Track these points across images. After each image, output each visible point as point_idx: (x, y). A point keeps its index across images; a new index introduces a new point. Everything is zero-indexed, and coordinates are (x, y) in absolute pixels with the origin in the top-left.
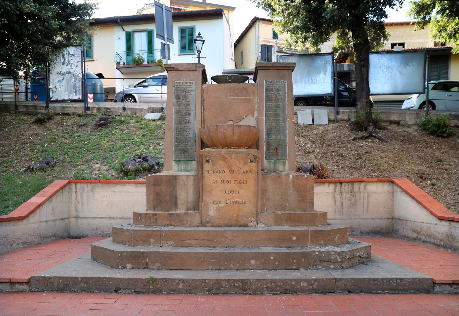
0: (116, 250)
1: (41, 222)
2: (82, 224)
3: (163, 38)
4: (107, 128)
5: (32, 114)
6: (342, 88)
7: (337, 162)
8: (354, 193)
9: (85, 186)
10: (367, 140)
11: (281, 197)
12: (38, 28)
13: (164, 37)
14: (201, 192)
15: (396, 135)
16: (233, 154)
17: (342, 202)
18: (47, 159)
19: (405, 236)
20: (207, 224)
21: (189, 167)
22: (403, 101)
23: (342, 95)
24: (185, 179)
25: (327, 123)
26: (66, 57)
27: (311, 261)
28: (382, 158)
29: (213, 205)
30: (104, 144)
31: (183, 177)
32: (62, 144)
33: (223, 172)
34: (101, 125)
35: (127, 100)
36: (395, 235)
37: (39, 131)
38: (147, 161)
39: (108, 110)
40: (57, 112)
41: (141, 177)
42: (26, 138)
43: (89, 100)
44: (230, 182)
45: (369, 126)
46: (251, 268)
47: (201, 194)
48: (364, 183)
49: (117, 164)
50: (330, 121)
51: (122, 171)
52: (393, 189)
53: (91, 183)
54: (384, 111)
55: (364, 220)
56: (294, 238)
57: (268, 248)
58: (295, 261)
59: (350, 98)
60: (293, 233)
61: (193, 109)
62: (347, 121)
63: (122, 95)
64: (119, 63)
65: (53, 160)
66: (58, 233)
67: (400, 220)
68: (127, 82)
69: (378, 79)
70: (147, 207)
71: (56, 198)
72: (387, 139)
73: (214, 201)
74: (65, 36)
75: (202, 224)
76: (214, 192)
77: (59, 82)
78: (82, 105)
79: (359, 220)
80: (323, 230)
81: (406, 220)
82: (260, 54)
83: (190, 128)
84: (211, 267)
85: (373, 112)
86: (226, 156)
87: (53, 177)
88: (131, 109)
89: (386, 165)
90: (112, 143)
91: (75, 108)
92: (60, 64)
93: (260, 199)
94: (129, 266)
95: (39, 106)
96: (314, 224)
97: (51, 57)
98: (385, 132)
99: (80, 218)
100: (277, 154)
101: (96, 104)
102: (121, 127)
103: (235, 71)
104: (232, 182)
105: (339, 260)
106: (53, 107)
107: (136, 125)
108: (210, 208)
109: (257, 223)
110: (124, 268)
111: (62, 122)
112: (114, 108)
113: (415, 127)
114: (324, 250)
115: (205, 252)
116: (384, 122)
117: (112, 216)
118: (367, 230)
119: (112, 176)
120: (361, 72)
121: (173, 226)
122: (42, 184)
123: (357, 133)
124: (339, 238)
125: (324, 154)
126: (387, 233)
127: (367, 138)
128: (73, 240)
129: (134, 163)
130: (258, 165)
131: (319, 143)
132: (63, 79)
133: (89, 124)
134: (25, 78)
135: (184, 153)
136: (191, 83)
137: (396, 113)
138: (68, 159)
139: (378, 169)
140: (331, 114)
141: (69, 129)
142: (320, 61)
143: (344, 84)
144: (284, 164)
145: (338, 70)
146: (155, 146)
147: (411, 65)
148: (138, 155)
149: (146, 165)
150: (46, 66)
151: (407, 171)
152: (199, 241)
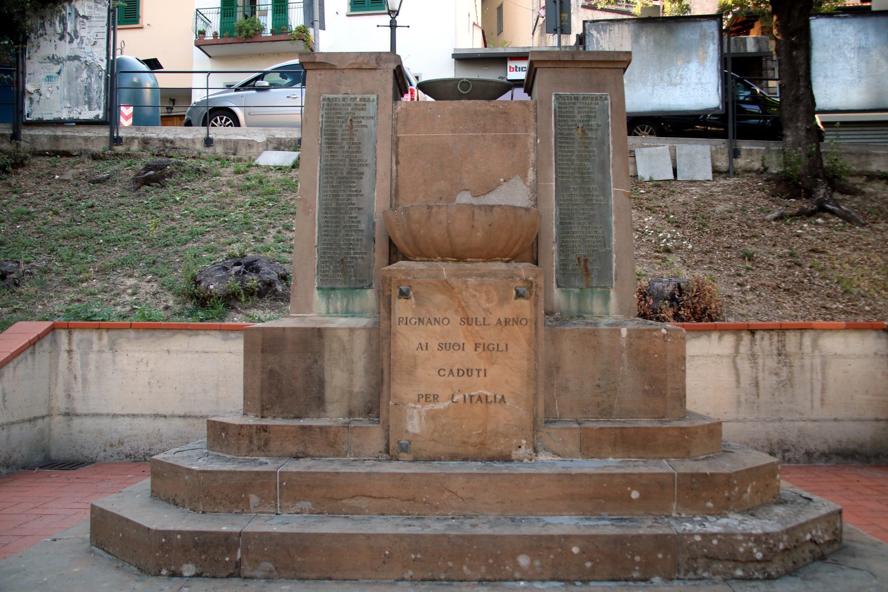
2: (81, 432)
4: (163, 186)
6: (744, 94)
7: (739, 275)
8: (786, 355)
9: (94, 335)
10: (812, 219)
11: (598, 382)
16: (470, 275)
17: (756, 378)
24: (344, 336)
25: (710, 177)
27: (682, 558)
28: (852, 264)
29: (419, 406)
30: (152, 227)
31: (340, 333)
32: (46, 227)
33: (446, 322)
34: (147, 181)
35: (216, 121)
38: (257, 270)
39: (169, 145)
40: (39, 148)
41: (239, 312)
43: (122, 120)
45: (816, 185)
46: (517, 575)
47: (386, 377)
48: (812, 332)
50: (716, 172)
51: (192, 296)
53: (108, 329)
56: (635, 495)
58: (637, 558)
59: (765, 119)
60: (631, 480)
61: (369, 161)
62: (759, 172)
64: (202, 33)
65: (19, 267)
66: (15, 456)
68: (218, 81)
69: (833, 76)
70: (245, 404)
71: (15, 368)
72: (865, 218)
73: (420, 396)
75: (389, 454)
76: (420, 372)
77: (49, 78)
78: (104, 132)
79: (802, 424)
80: (712, 474)
82: (543, 13)
83: (359, 209)
84: (411, 573)
85: (826, 153)
86: (453, 281)
87: (14, 311)
88: (225, 142)
89: (865, 284)
90: (173, 224)
91: (86, 139)
92: (53, 38)
93: (541, 389)
94: (189, 569)
96: (687, 455)
97: (29, 23)
98: (858, 199)
99: (77, 415)
100: (587, 273)
101: (138, 130)
102: (197, 185)
104: (470, 347)
105: (759, 556)
106: (31, 136)
107: (236, 180)
108: (409, 412)
109: (536, 451)
110: (174, 574)
111: (49, 174)
112: (182, 140)
114: (716, 529)
115: (395, 535)
116: (853, 175)
117: (162, 411)
118: (823, 448)
119: (167, 308)
120: (791, 60)
121: (312, 457)
123: (787, 202)
124: (756, 491)
125: (706, 252)
126: (877, 456)
127: (811, 214)
128: (55, 474)
129: (223, 277)
130: (536, 305)
131: (693, 227)
132: (59, 73)
135: (343, 270)
136: (364, 100)
137: (884, 155)
138: (57, 266)
139: (846, 292)
140: (719, 156)
141: (66, 190)
142: (688, 33)
143: (748, 87)
144: (606, 298)
145: (733, 50)
146: (279, 232)
148: (234, 257)
149: (253, 280)
150: (17, 43)
152: (381, 502)
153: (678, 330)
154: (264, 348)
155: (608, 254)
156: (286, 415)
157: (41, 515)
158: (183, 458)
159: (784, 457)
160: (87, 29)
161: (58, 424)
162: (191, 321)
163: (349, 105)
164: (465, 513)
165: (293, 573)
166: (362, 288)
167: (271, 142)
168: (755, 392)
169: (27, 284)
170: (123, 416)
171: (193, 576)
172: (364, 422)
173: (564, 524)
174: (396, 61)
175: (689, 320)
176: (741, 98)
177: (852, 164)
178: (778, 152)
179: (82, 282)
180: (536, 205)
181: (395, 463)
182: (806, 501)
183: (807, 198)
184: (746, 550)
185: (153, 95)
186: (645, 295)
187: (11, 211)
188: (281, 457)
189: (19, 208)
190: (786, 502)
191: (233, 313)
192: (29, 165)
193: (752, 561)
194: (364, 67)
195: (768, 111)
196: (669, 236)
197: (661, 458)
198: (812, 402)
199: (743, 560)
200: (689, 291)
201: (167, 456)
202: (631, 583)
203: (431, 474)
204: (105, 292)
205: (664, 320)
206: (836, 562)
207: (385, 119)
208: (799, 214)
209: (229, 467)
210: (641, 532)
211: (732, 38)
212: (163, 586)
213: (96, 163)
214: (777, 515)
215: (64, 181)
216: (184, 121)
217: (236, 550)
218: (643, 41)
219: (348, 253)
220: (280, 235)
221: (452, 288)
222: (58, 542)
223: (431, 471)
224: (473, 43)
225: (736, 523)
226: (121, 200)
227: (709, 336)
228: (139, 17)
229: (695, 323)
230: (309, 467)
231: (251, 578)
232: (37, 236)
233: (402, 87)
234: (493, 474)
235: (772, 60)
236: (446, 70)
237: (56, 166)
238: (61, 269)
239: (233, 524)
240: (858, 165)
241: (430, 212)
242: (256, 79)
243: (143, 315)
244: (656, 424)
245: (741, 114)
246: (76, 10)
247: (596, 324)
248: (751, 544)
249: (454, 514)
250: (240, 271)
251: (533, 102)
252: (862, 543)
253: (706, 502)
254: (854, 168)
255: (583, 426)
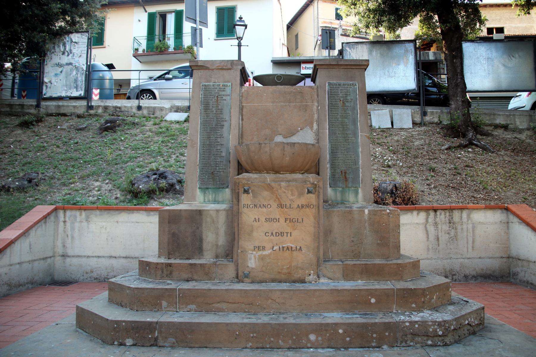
0: (110, 318)
1: (11, 265)
2: (70, 265)
3: (195, 21)
4: (115, 132)
5: (17, 115)
6: (428, 82)
7: (428, 180)
8: (453, 223)
9: (78, 213)
10: (466, 149)
11: (352, 239)
12: (33, 12)
13: (196, 21)
14: (236, 234)
15: (504, 142)
16: (282, 181)
17: (438, 236)
18: (30, 175)
19: (528, 282)
20: (245, 279)
21: (220, 197)
22: (510, 98)
23: (428, 91)
24: (213, 214)
26: (67, 46)
27: (399, 335)
28: (487, 173)
29: (254, 253)
31: (211, 213)
32: (52, 154)
33: (269, 206)
34: (106, 129)
35: (144, 97)
36: (512, 280)
37: (24, 137)
38: (166, 178)
39: (118, 110)
40: (50, 112)
41: (156, 201)
42: (5, 147)
43: (94, 96)
44: (278, 220)
45: (468, 131)
46: (309, 345)
48: (467, 210)
49: (124, 182)
50: (414, 123)
51: (130, 192)
52: (508, 217)
53: (85, 209)
54: (487, 111)
55: (469, 260)
56: (373, 301)
57: (335, 314)
58: (375, 335)
59: (440, 95)
60: (371, 293)
62: (437, 124)
63: (138, 91)
64: (137, 50)
65: (38, 176)
66: (36, 278)
67: (519, 260)
68: (145, 75)
69: (475, 73)
70: (159, 251)
71: (36, 231)
72: (494, 148)
74: (69, 21)
75: (238, 279)
76: (255, 234)
78: (84, 103)
79: (462, 260)
80: (415, 289)
81: (529, 261)
82: (320, 38)
83: (222, 145)
84: (250, 344)
85: (473, 114)
86: (273, 184)
87: (36, 200)
88: (148, 108)
89: (494, 184)
90: (120, 152)
91: (75, 107)
92: (59, 54)
93: (321, 243)
94: (129, 342)
95: (27, 105)
96: (401, 279)
97: (47, 46)
98: (490, 138)
99: (68, 256)
100: (346, 179)
101: (102, 102)
102: (134, 131)
103: (288, 59)
104: (282, 220)
105: (440, 333)
106: (46, 105)
107: (154, 128)
108: (249, 256)
109: (318, 277)
110: (121, 344)
111: (55, 125)
112: (125, 107)
113: (529, 133)
114: (417, 319)
115: (241, 324)
117: (114, 255)
118: (474, 273)
119: (116, 198)
121: (196, 280)
122: (20, 209)
123: (452, 140)
125: (410, 167)
126: (502, 277)
127: (466, 146)
128: (57, 288)
129: (147, 181)
130: (318, 197)
132: (61, 72)
133: (91, 128)
134: (13, 71)
135: (212, 178)
136: (224, 86)
137: (503, 115)
141: (64, 134)
142: (398, 50)
143: (430, 78)
144: (357, 193)
145: (422, 59)
147: (517, 56)
148: (153, 170)
149: (163, 183)
150: (41, 57)
151: (523, 192)
152: (234, 305)
153: (396, 211)
154: (169, 220)
155: (357, 169)
156: (181, 257)
157: (50, 311)
158: (126, 280)
159: (452, 279)
160: (77, 49)
161: (58, 260)
162: (129, 206)
163: (216, 88)
164: (280, 311)
165: (186, 344)
166: (223, 188)
167: (173, 108)
168: (437, 243)
169: (43, 185)
170: (93, 257)
171: (132, 345)
172: (224, 262)
173: (334, 317)
174: (241, 65)
175: (401, 204)
176: (427, 84)
177: (486, 120)
178: (447, 113)
179: (72, 184)
180: (318, 143)
181: (242, 284)
182: (465, 302)
183: (463, 138)
184: (433, 330)
185: (110, 83)
186: (377, 191)
187: (35, 145)
188: (179, 280)
189: (39, 144)
190: (455, 303)
191: (152, 201)
192: (44, 121)
193: (436, 336)
194: (225, 68)
195: (442, 91)
196: (389, 158)
197: (387, 280)
198: (467, 248)
199: (432, 335)
200: (401, 188)
201: (117, 279)
202: (371, 349)
203: (261, 290)
204: (84, 189)
205: (387, 204)
206: (481, 335)
207: (236, 96)
208: (459, 146)
209: (150, 286)
210: (377, 321)
211: (422, 52)
212: (115, 351)
213: (79, 120)
214: (450, 310)
215: (62, 129)
216: (126, 97)
217: (155, 331)
218: (374, 53)
219: (216, 169)
220: (178, 158)
221: (273, 188)
222: (59, 325)
223: (261, 289)
224: (282, 54)
225: (428, 315)
226: (92, 139)
227: (412, 213)
228: (104, 42)
229: (404, 206)
230: (194, 286)
231: (163, 347)
232: (48, 159)
233: (245, 79)
234: (296, 290)
235: (443, 64)
236: (268, 70)
237: (58, 121)
238: (60, 177)
239: (153, 317)
240: (489, 120)
241: (261, 147)
242: (166, 74)
243: (104, 202)
244: (384, 262)
245: (427, 92)
246: (71, 39)
247: (351, 207)
248: (436, 327)
249: (274, 312)
250: (156, 178)
251: (316, 87)
252: (494, 324)
253: (411, 304)
254: (487, 122)
255: (344, 263)
